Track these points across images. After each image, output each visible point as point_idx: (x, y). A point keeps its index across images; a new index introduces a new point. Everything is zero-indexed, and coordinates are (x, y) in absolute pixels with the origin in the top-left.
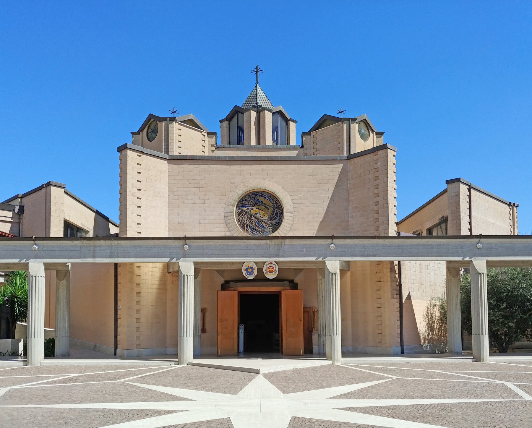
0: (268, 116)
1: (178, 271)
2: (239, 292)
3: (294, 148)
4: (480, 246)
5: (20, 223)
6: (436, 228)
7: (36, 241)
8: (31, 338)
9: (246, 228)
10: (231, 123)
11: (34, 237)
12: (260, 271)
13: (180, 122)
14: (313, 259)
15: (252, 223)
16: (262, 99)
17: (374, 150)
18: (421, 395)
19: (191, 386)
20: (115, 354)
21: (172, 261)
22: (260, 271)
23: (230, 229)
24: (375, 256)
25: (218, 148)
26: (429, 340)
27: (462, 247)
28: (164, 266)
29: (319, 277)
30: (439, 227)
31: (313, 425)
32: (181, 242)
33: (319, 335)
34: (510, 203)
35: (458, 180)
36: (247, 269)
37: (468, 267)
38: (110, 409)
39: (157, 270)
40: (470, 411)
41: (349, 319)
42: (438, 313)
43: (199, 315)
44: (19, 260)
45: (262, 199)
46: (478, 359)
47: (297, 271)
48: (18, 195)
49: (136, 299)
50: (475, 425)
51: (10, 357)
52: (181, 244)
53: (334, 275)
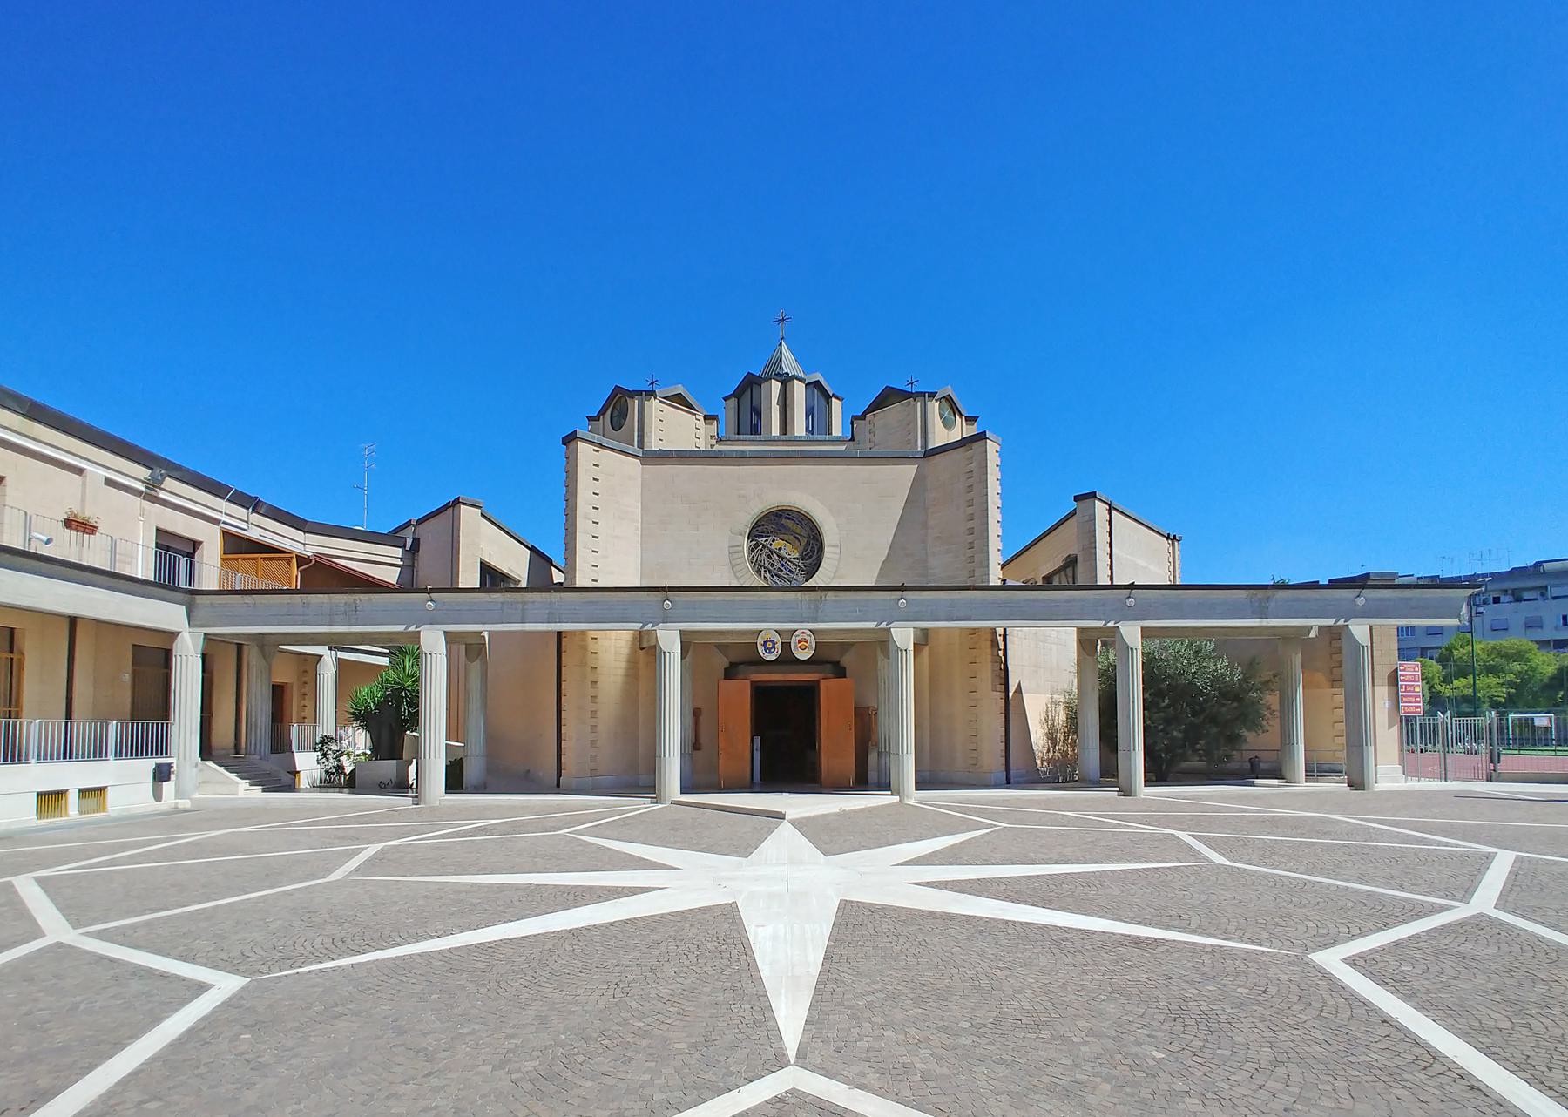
0: (799, 389)
1: (655, 646)
2: (752, 683)
3: (838, 441)
4: (1131, 602)
5: (413, 566)
6: (1058, 575)
7: (431, 595)
8: (425, 757)
9: (763, 573)
10: (741, 400)
11: (429, 587)
12: (786, 646)
13: (664, 398)
14: (872, 625)
15: (773, 565)
16: (790, 364)
17: (966, 442)
18: (1048, 857)
19: (675, 842)
20: (558, 786)
21: (645, 628)
22: (786, 646)
23: (739, 575)
24: (969, 619)
25: (721, 440)
26: (1049, 761)
27: (1103, 605)
28: (634, 638)
29: (880, 656)
30: (1062, 573)
31: (877, 917)
32: (659, 596)
33: (879, 754)
34: (1169, 534)
35: (1093, 495)
36: (765, 642)
37: (1111, 638)
38: (539, 885)
39: (623, 643)
40: (1133, 886)
41: (926, 724)
42: (1062, 716)
43: (690, 720)
44: (405, 626)
45: (789, 523)
46: (1126, 792)
47: (845, 647)
48: (410, 521)
49: (591, 692)
50: (1148, 914)
51: (395, 790)
52: (660, 599)
53: (904, 652)
